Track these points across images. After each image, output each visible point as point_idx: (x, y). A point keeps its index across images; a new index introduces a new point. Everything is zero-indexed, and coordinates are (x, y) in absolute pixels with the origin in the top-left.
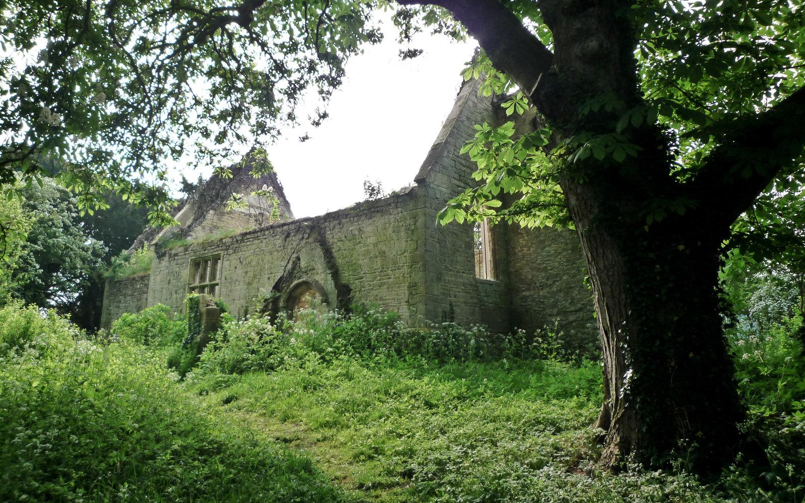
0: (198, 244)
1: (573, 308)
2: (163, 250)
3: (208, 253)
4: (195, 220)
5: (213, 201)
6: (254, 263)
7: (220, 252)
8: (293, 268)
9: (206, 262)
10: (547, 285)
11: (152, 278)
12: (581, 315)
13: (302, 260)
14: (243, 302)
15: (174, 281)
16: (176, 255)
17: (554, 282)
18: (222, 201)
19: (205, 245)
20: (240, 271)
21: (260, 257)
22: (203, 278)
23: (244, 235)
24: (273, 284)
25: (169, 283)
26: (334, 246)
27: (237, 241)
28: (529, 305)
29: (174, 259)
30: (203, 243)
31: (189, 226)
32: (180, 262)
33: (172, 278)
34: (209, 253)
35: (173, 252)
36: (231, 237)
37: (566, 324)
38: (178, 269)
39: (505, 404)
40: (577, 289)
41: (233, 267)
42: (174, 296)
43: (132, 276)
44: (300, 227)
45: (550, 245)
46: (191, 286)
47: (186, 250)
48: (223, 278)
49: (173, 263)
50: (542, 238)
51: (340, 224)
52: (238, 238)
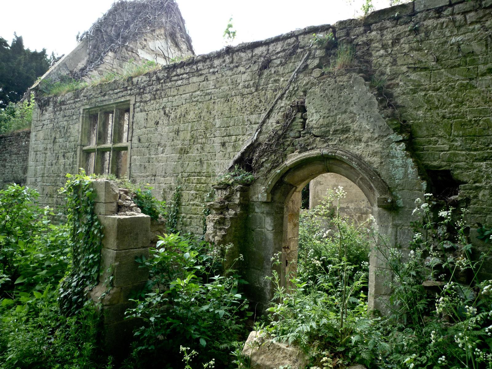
0: (93, 87)
2: (46, 97)
3: (110, 100)
4: (90, 62)
5: (112, 41)
6: (191, 116)
7: (128, 98)
8: (287, 128)
9: (107, 114)
11: (33, 135)
13: (310, 109)
14: (172, 181)
15: (61, 140)
16: (63, 103)
18: (124, 42)
19: (102, 89)
20: (164, 129)
21: (204, 105)
22: (102, 138)
23: (170, 69)
24: (238, 155)
25: (54, 142)
27: (158, 79)
29: (61, 110)
30: (101, 85)
31: (82, 70)
32: (68, 113)
33: (58, 136)
34: (111, 100)
35: (59, 99)
36: (148, 74)
38: (65, 123)
41: (151, 123)
42: (62, 161)
43: (16, 132)
44: (296, 47)
46: (85, 148)
47: (77, 95)
48: (135, 140)
49: (60, 115)
51: (415, 31)
52: (160, 75)
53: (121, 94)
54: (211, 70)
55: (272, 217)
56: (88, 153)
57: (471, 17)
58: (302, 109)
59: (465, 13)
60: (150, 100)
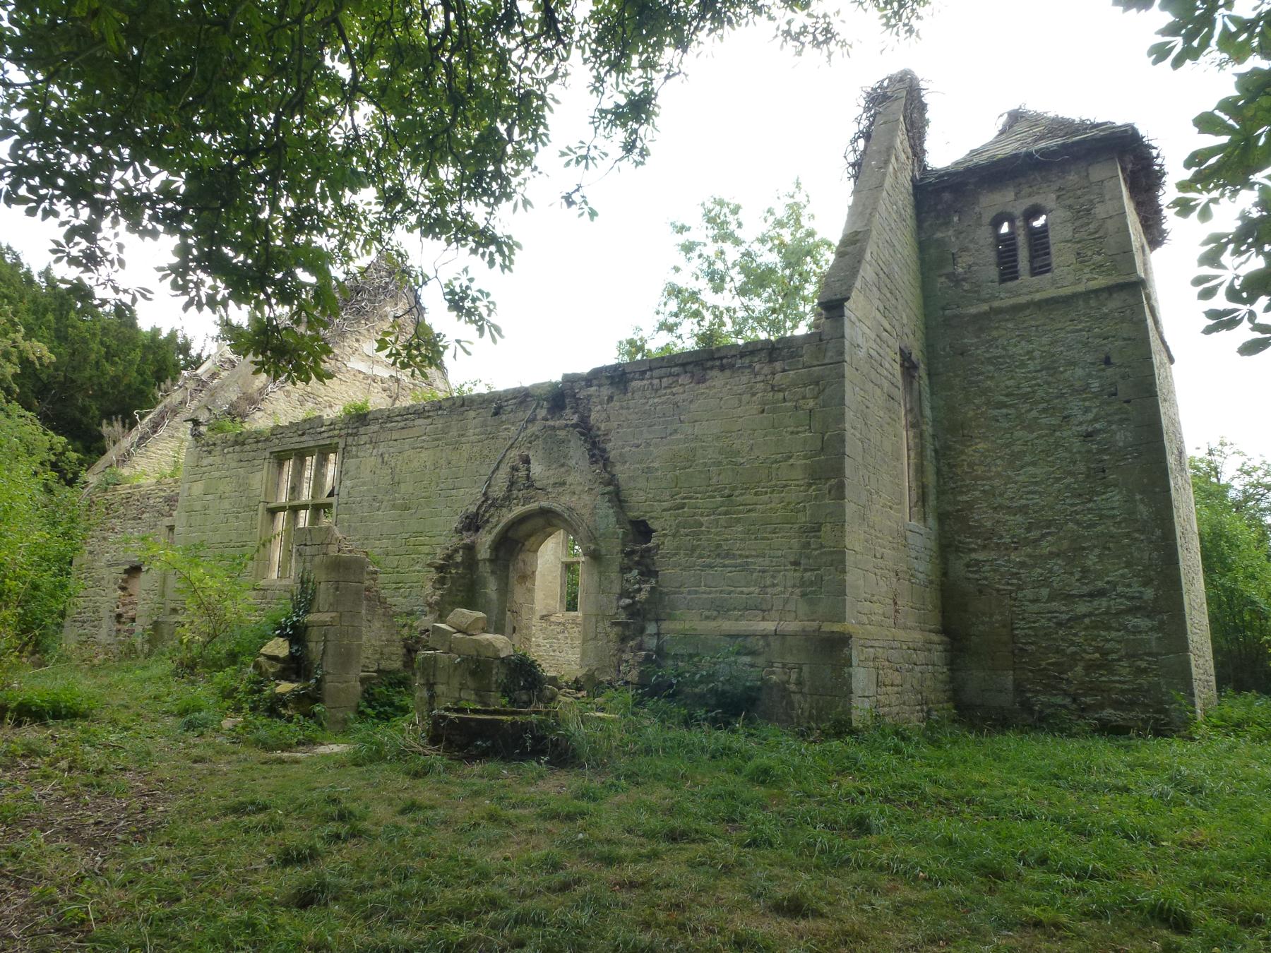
1: (1086, 589)
7: (336, 440)
10: (1027, 542)
12: (1104, 604)
17: (1043, 536)
26: (612, 436)
28: (986, 579)
37: (1069, 620)
39: (144, 668)
40: (1097, 551)
45: (1034, 464)
50: (1017, 448)
53: (326, 435)
54: (440, 412)
55: (143, 333)
56: (273, 512)
57: (665, 382)
58: (527, 461)
59: (660, 378)
60: (365, 444)
